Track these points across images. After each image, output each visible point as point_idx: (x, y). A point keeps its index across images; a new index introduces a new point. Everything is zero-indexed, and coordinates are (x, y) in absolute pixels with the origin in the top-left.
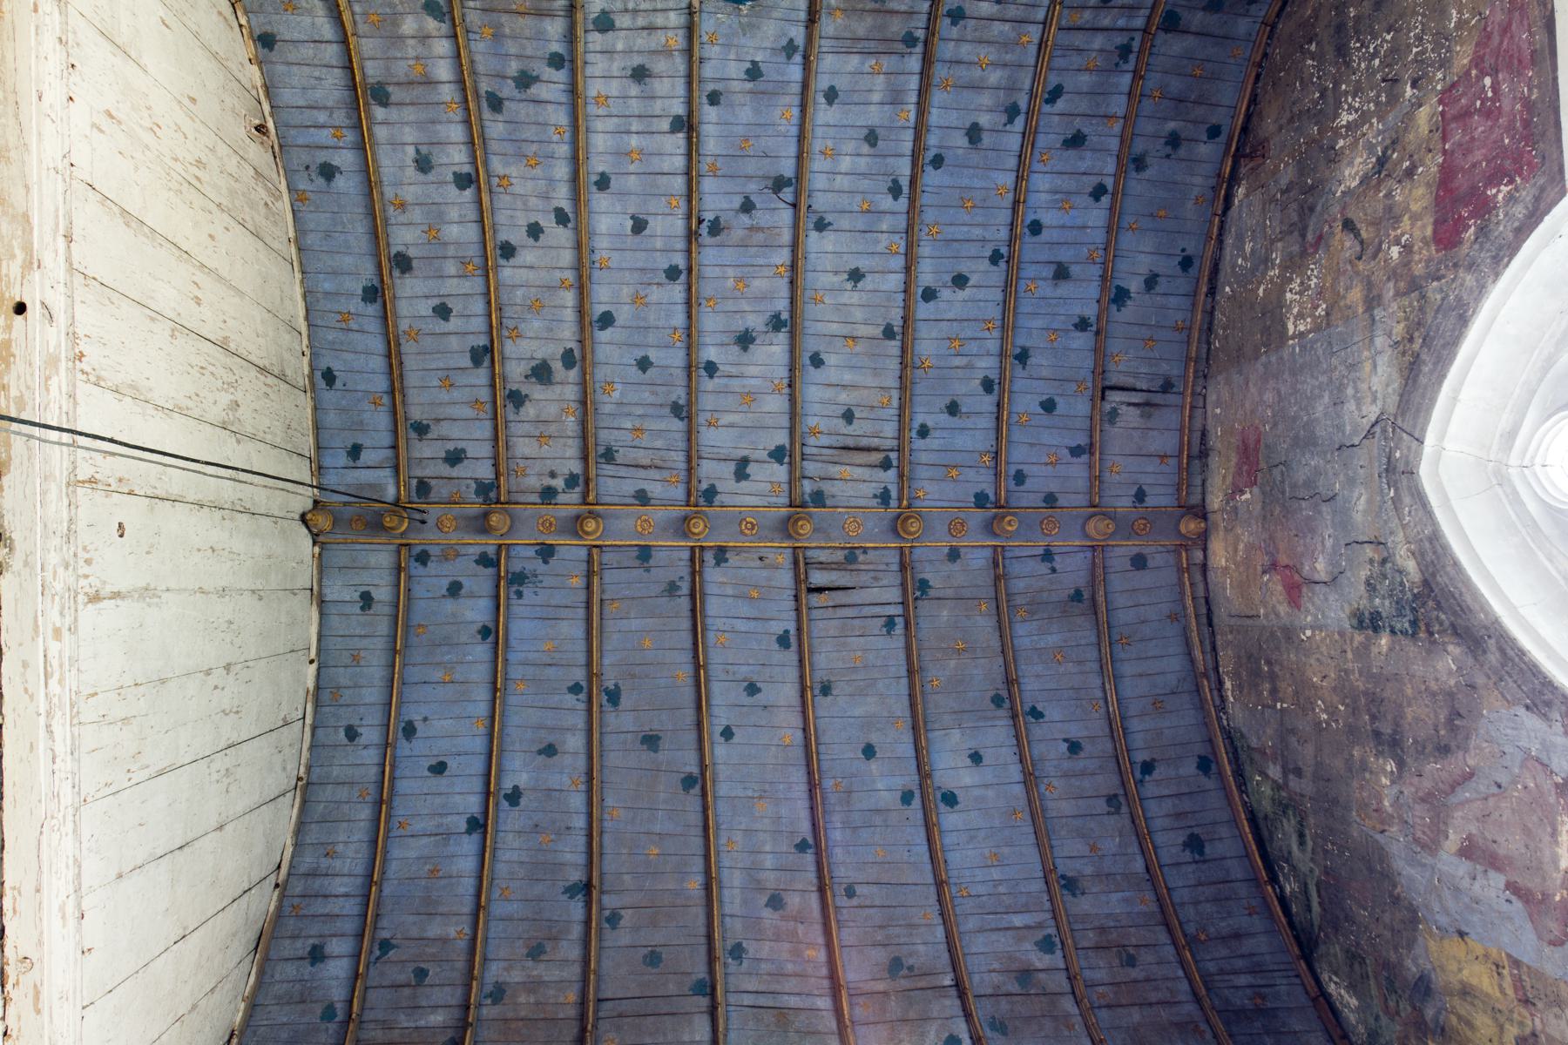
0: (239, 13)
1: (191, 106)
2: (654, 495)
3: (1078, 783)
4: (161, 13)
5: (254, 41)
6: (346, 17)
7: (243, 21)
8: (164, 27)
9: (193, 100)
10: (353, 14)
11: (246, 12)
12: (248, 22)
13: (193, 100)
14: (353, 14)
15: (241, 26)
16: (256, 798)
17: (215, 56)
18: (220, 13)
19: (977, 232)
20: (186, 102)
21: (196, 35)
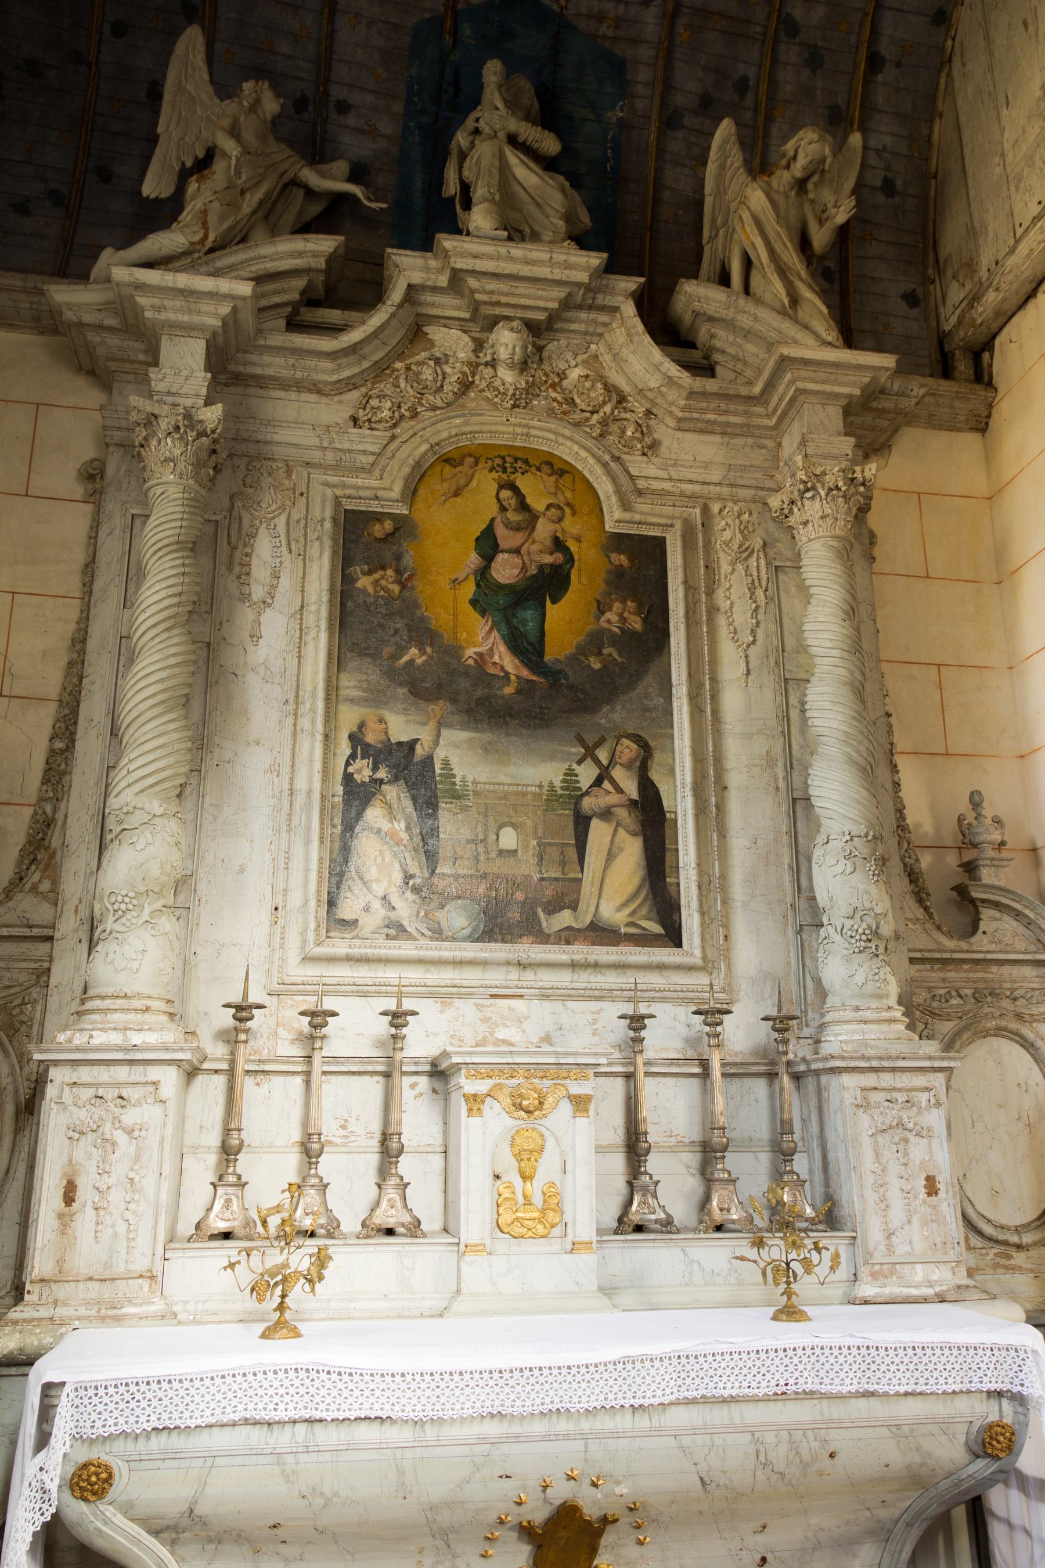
0: (949, 51)
1: (1030, 21)
2: (800, 311)
3: (814, 1520)
4: (1005, 112)
5: (950, 19)
6: (866, 34)
7: (949, 42)
8: (1011, 101)
9: (1025, 23)
10: (859, 35)
11: (943, 49)
12: (945, 40)
13: (1025, 23)
14: (859, 35)
15: (954, 39)
16: (1040, 752)
17: (987, 37)
18: (964, 65)
19: (558, 274)
20: (1031, 29)
21: (991, 68)
